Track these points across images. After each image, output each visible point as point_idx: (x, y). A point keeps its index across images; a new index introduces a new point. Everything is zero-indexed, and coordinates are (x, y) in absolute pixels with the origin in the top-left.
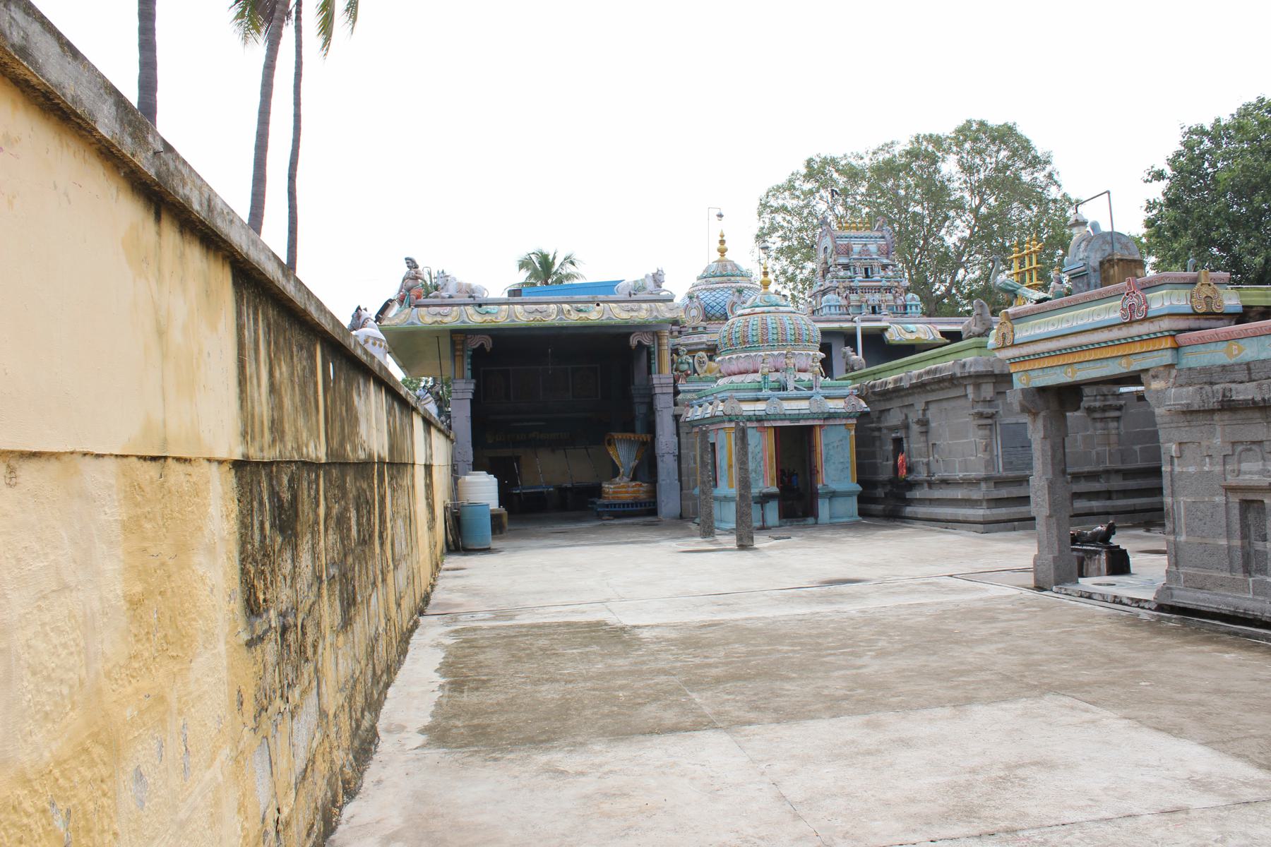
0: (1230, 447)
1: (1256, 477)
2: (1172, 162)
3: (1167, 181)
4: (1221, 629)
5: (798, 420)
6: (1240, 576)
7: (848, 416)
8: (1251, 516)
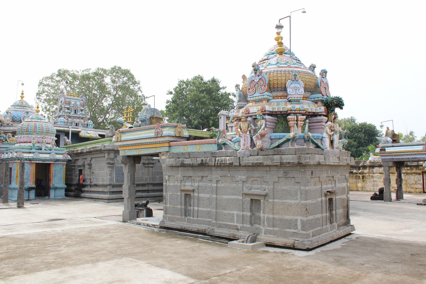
1: (189, 187)
2: (175, 89)
3: (173, 95)
6: (183, 217)
7: (63, 161)
8: (187, 199)
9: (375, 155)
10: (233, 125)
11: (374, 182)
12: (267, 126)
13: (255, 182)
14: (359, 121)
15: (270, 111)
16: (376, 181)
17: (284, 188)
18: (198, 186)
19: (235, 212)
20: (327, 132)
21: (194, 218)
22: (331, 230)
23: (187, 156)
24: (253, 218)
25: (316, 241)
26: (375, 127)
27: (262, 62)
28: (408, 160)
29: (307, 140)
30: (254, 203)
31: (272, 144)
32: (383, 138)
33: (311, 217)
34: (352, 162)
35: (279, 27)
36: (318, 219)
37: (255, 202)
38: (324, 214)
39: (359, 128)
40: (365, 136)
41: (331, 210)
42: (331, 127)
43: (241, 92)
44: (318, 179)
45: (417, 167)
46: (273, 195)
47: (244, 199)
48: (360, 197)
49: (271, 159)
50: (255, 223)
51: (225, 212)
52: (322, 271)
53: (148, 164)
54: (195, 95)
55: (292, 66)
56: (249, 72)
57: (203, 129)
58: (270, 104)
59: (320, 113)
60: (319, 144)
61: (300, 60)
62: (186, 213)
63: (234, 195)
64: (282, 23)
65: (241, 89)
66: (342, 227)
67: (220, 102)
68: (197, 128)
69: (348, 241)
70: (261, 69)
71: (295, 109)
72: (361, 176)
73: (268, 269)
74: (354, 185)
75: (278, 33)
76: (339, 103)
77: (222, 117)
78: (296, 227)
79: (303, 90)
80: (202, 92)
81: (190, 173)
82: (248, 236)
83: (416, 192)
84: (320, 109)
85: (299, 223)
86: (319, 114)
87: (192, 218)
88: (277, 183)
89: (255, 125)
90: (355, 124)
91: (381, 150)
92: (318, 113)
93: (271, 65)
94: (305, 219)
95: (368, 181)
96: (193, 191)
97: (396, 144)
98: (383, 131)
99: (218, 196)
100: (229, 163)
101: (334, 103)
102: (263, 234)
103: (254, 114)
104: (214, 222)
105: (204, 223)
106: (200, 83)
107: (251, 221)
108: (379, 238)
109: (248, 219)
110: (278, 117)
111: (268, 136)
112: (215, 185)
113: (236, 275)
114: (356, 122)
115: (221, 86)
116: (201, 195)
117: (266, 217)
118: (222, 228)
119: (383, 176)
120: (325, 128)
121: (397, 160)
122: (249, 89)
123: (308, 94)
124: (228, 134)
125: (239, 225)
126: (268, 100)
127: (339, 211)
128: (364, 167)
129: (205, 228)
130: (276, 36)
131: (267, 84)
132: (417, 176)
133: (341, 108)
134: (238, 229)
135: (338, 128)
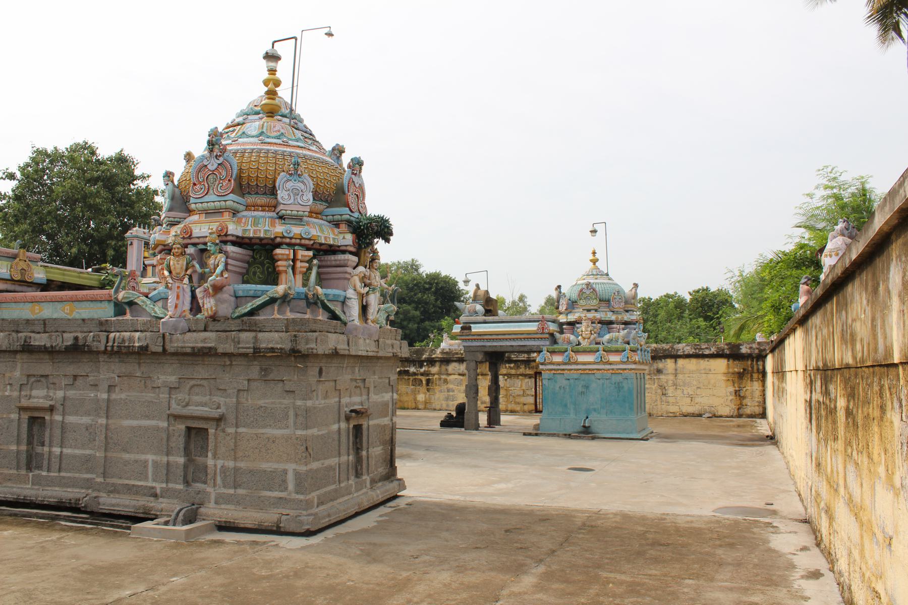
0: (25, 379)
1: (41, 401)
2: (22, 169)
3: (16, 182)
4: (5, 513)
6: (23, 472)
8: (35, 429)
9: (453, 337)
10: (154, 261)
11: (448, 391)
12: (229, 267)
13: (196, 390)
14: (427, 269)
15: (237, 237)
16: (452, 390)
17: (261, 402)
18: (65, 398)
19: (150, 457)
20: (355, 287)
21: (52, 474)
22: (357, 491)
23: (39, 328)
24: (191, 470)
25: (325, 513)
26: (455, 283)
27: (231, 129)
28: (510, 349)
29: (314, 302)
30: (193, 436)
31: (237, 307)
32: (470, 308)
33: (315, 465)
34: (405, 351)
35: (272, 57)
36: (330, 468)
37: (196, 435)
38: (344, 458)
39: (425, 283)
40: (436, 300)
41: (358, 449)
42: (365, 276)
43: (177, 190)
44: (332, 384)
45: (528, 362)
46: (237, 418)
47: (171, 428)
48: (419, 422)
49: (233, 340)
50: (194, 481)
51: (126, 456)
52: (335, 576)
54: (73, 187)
55: (291, 143)
56: (200, 149)
57: (86, 269)
58: (239, 222)
59: (344, 248)
60: (338, 311)
61: (313, 133)
62: (31, 462)
63: (149, 419)
64: (280, 49)
65: (176, 183)
66: (380, 484)
67: (133, 208)
68: (74, 262)
69: (392, 512)
70: (224, 142)
71: (291, 235)
72: (424, 379)
73: (220, 580)
74: (411, 398)
75: (272, 71)
76: (383, 229)
77: (135, 242)
78: (283, 486)
79: (310, 196)
80: (93, 181)
81: (45, 367)
82: (178, 509)
83: (524, 412)
84: (344, 238)
85: (290, 477)
86: (342, 248)
87: (44, 473)
88: (245, 393)
89: (203, 265)
90: (419, 274)
91: (463, 328)
92: (339, 246)
93: (248, 136)
94: (303, 468)
95: (437, 388)
96: (51, 409)
97: (490, 318)
98: (470, 290)
99: (110, 421)
100: (139, 347)
101: (373, 229)
102: (212, 505)
103: (202, 240)
104: (100, 480)
105: (73, 483)
106: (88, 162)
107: (185, 477)
108: (450, 502)
109: (180, 472)
110: (253, 250)
111: (229, 289)
112: (105, 396)
113: (145, 601)
114: (421, 270)
115: (137, 172)
116: (71, 419)
117: (219, 467)
118: (118, 493)
119: (465, 380)
120: (352, 280)
121: (491, 350)
122: (195, 184)
123: (320, 206)
124: (145, 280)
125: (159, 486)
126: (235, 213)
127: (376, 451)
128: (431, 362)
129: (78, 496)
131: (234, 176)
132: (527, 380)
133: (387, 241)
134: (155, 496)
135: (377, 280)
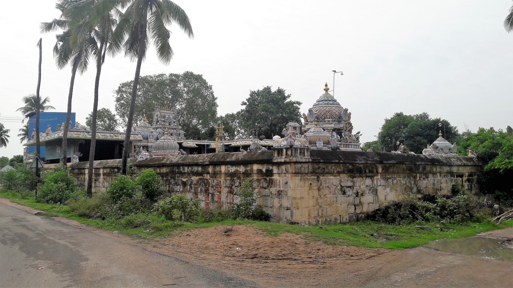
5: (154, 162)
39: (431, 125)
53: (245, 163)
114: (430, 118)
115: (286, 95)
130: (324, 87)
